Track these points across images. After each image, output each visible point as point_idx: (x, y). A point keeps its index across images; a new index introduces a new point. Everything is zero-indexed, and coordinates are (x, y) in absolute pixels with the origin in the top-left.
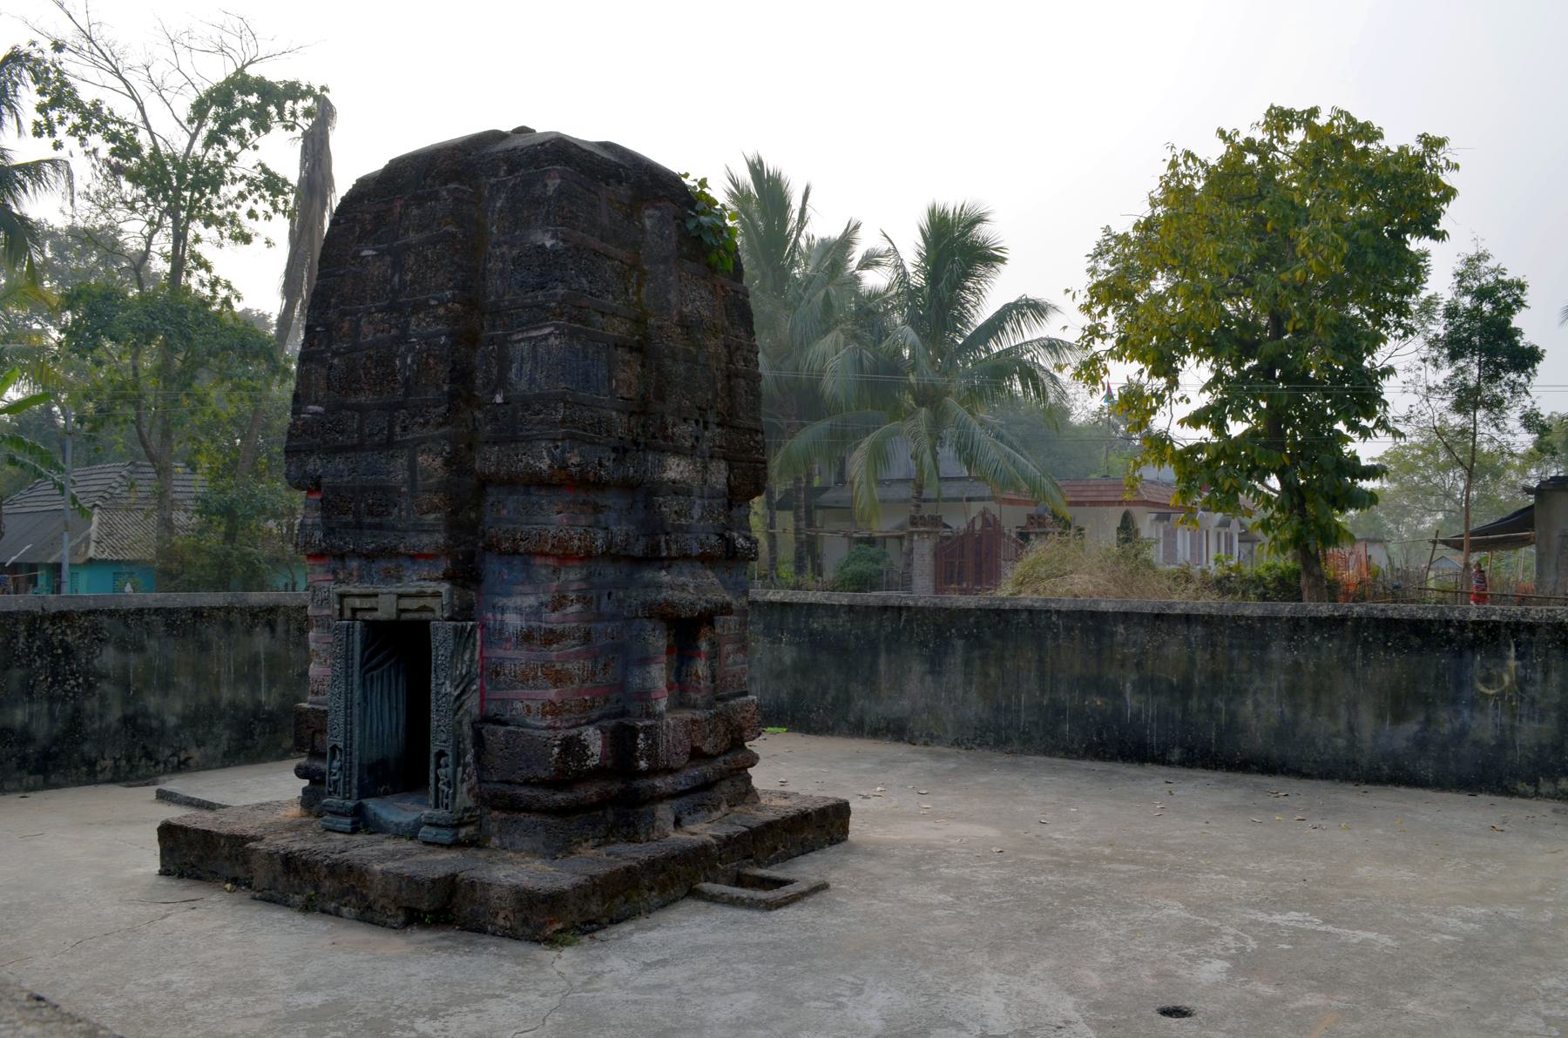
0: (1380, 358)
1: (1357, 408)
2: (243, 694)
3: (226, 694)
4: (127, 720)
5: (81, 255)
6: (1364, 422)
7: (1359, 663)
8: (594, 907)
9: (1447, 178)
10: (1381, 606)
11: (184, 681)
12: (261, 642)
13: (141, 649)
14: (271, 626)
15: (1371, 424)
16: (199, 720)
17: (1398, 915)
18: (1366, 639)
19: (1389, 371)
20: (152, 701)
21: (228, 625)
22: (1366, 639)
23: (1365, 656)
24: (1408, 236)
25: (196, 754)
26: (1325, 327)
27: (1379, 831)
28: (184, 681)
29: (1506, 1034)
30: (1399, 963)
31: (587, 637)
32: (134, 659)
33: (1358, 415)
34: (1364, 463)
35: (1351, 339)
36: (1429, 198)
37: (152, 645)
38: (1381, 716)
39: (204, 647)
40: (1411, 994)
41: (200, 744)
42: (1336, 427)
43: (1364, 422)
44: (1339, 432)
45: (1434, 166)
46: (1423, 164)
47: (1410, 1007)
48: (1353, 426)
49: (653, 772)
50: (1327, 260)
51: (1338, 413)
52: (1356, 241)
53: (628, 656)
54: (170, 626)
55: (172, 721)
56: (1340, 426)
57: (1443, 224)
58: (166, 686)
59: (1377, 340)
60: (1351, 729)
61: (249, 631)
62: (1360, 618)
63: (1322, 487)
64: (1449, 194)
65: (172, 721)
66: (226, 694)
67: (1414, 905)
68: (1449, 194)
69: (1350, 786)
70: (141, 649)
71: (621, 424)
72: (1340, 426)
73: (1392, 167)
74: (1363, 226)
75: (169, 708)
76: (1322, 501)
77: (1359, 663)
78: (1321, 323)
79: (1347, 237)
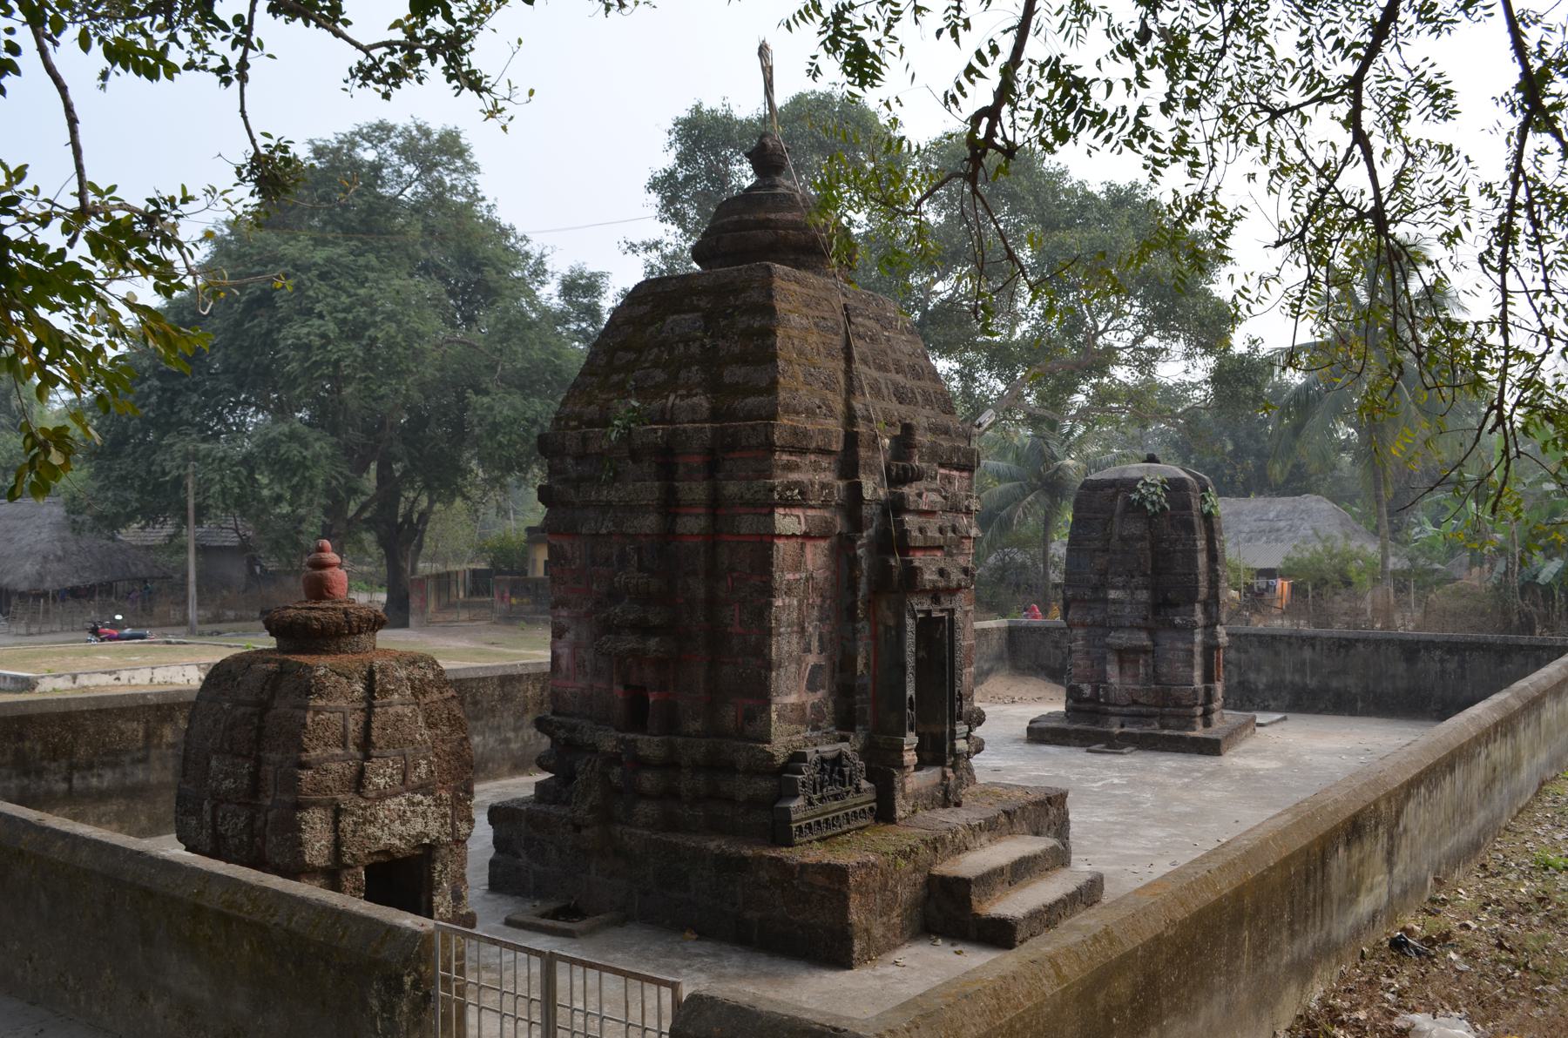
2: (1297, 678)
3: (1288, 677)
4: (1240, 683)
8: (1047, 737)
11: (1267, 668)
12: (1307, 654)
13: (1246, 652)
14: (1313, 647)
16: (1275, 688)
20: (1252, 676)
21: (1290, 644)
25: (1273, 704)
28: (1267, 668)
29: (5, 385)
31: (1088, 653)
32: (1243, 656)
37: (1252, 650)
39: (1277, 654)
41: (1275, 699)
49: (1107, 704)
53: (1103, 660)
54: (1260, 642)
55: (1261, 687)
58: (1258, 670)
61: (1301, 648)
65: (1261, 687)
66: (1288, 677)
70: (1246, 652)
71: (1094, 579)
75: (1262, 681)
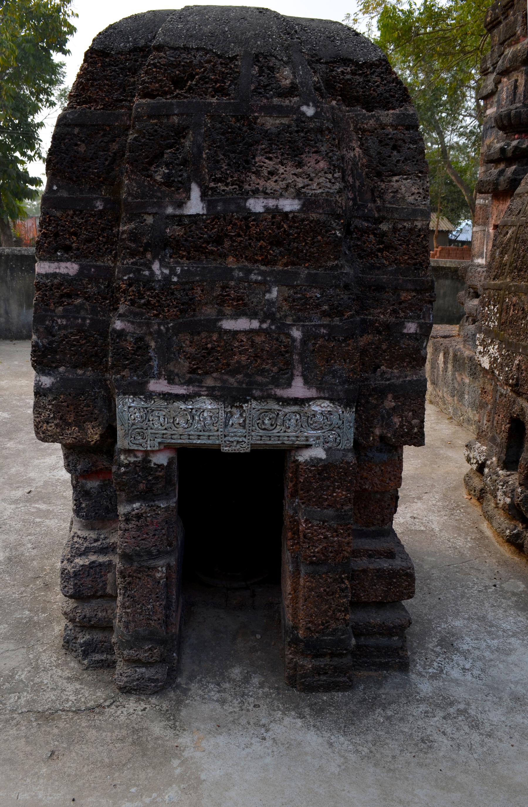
0: (37, 118)
1: (25, 144)
5: (206, 56)
6: (29, 152)
7: (9, 279)
9: (72, 21)
10: (19, 248)
15: (32, 154)
17: (14, 402)
18: (12, 266)
19: (41, 125)
22: (12, 266)
23: (12, 274)
24: (51, 52)
26: (8, 97)
27: (16, 363)
30: (8, 425)
33: (28, 148)
34: (31, 176)
35: (21, 106)
36: (61, 31)
38: (21, 306)
40: (10, 439)
42: (15, 155)
43: (29, 152)
44: (16, 158)
45: (65, 13)
46: (59, 11)
47: (8, 445)
48: (24, 154)
50: (8, 57)
51: (16, 147)
52: (23, 50)
56: (17, 154)
57: (68, 47)
59: (35, 109)
60: (7, 313)
62: (8, 255)
63: (9, 186)
64: (72, 30)
67: (23, 397)
68: (72, 30)
69: (8, 342)
72: (17, 154)
73: (42, 10)
74: (28, 41)
76: (10, 195)
77: (9, 279)
78: (6, 94)
79: (19, 46)
